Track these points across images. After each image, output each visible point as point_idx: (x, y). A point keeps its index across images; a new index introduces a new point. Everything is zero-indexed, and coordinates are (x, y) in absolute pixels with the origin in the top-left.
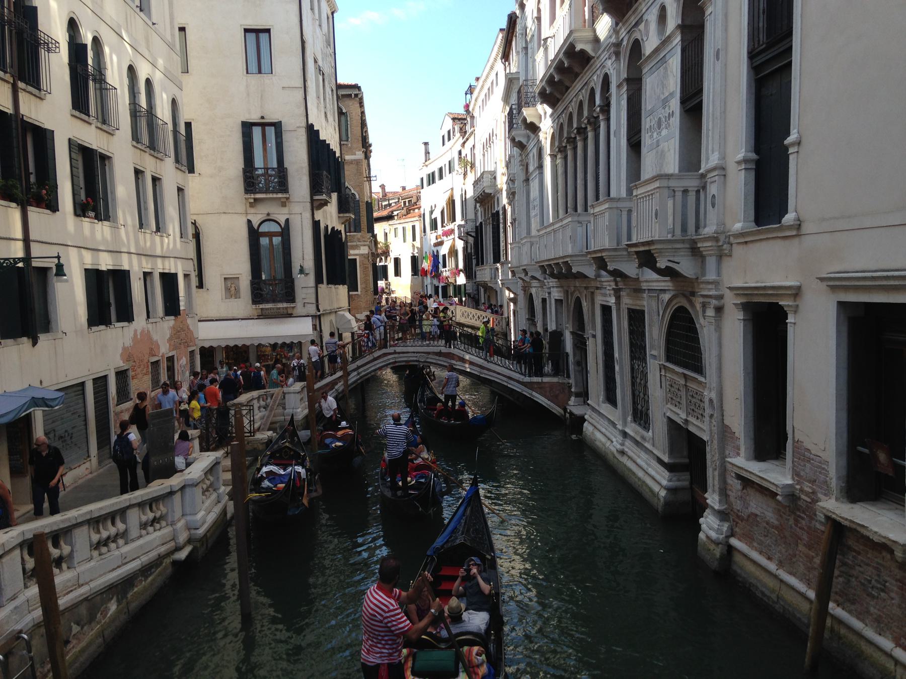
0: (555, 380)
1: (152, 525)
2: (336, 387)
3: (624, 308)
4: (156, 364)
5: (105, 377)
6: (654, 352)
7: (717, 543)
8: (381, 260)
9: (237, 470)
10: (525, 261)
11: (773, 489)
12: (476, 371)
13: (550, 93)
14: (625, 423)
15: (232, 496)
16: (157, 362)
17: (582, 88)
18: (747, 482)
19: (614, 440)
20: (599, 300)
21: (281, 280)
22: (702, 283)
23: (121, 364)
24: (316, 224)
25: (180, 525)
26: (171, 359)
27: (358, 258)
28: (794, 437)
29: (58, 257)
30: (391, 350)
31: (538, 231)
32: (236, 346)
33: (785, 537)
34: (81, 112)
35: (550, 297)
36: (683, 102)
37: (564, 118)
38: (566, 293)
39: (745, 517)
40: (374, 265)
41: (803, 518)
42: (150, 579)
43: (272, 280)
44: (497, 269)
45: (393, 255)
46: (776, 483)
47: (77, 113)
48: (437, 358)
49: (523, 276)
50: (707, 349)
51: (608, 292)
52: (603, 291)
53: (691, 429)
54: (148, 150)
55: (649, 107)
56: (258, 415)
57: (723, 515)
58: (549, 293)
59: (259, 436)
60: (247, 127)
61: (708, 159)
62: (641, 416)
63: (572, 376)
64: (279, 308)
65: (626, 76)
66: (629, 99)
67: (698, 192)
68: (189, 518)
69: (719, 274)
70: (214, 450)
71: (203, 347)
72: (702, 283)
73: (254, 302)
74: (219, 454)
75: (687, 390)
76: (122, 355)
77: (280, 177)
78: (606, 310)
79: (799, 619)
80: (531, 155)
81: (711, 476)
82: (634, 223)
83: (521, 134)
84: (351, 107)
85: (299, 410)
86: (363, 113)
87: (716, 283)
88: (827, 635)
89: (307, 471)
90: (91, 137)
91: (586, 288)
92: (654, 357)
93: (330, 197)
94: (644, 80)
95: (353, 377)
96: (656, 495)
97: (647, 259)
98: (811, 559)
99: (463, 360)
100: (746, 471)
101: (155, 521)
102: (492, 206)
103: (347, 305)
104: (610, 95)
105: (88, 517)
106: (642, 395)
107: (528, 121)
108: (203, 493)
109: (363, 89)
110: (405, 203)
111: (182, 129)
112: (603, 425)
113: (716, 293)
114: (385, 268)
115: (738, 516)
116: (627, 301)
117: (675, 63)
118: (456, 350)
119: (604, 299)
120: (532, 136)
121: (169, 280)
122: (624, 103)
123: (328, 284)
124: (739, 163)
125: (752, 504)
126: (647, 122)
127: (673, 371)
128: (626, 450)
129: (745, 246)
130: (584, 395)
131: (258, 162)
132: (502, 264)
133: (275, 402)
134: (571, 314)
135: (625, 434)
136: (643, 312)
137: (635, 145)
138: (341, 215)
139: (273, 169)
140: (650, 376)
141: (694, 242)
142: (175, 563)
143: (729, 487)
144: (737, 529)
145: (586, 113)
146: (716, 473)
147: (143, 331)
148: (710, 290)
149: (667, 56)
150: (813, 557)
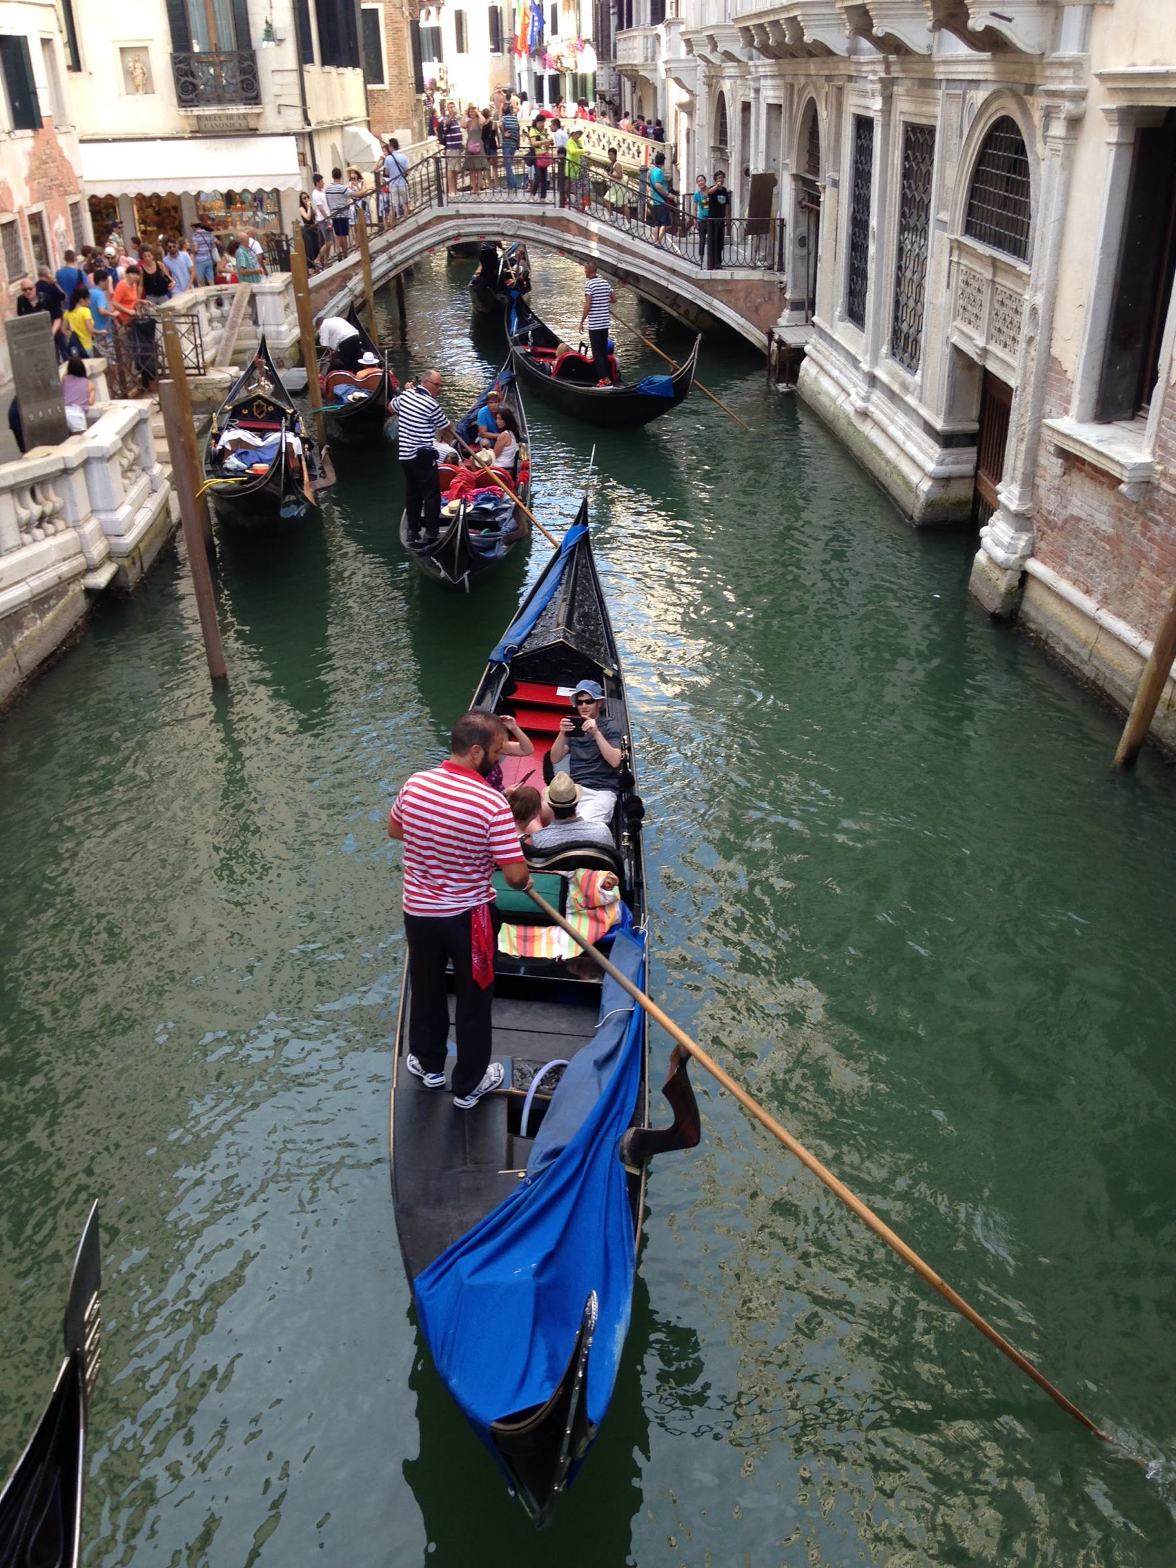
0: (757, 275)
1: (39, 526)
2: (350, 284)
3: (898, 120)
6: (944, 216)
7: (1004, 568)
9: (176, 432)
10: (713, 19)
11: (1116, 472)
12: (610, 256)
14: (875, 360)
15: (176, 481)
16: (11, 224)
18: (1072, 461)
19: (852, 391)
20: (853, 105)
21: (230, 54)
22: (1052, 64)
25: (90, 527)
26: (36, 219)
28: (1168, 378)
30: (449, 210)
32: (156, 196)
33: (1121, 556)
35: (757, 99)
39: (1060, 523)
40: (415, 24)
41: (1157, 523)
42: (49, 616)
43: (213, 55)
44: (658, 37)
46: (1122, 460)
50: (1041, 205)
51: (869, 87)
52: (860, 85)
53: (992, 367)
56: (210, 335)
57: (1022, 521)
59: (214, 375)
62: (905, 345)
63: (788, 267)
64: (231, 117)
68: (103, 516)
69: (1084, 45)
70: (138, 396)
71: (93, 197)
72: (1052, 64)
73: (183, 102)
74: (144, 404)
75: (995, 290)
79: (1120, 688)
85: (284, 328)
87: (1076, 65)
88: (1159, 712)
89: (304, 441)
91: (829, 78)
92: (943, 224)
95: (381, 265)
96: (911, 489)
98: (1156, 591)
99: (586, 233)
100: (1076, 441)
101: (43, 520)
103: (364, 112)
106: (911, 303)
112: (835, 364)
113: (1075, 87)
114: (436, 33)
115: (1047, 522)
116: (905, 108)
119: (862, 102)
123: (324, 63)
125: (1075, 500)
128: (872, 409)
130: (806, 306)
132: (668, 26)
133: (238, 308)
134: (796, 140)
135: (873, 380)
140: (930, 265)
142: (89, 592)
143: (1040, 472)
144: (1042, 545)
146: (1023, 447)
148: (1063, 79)
150: (1162, 588)
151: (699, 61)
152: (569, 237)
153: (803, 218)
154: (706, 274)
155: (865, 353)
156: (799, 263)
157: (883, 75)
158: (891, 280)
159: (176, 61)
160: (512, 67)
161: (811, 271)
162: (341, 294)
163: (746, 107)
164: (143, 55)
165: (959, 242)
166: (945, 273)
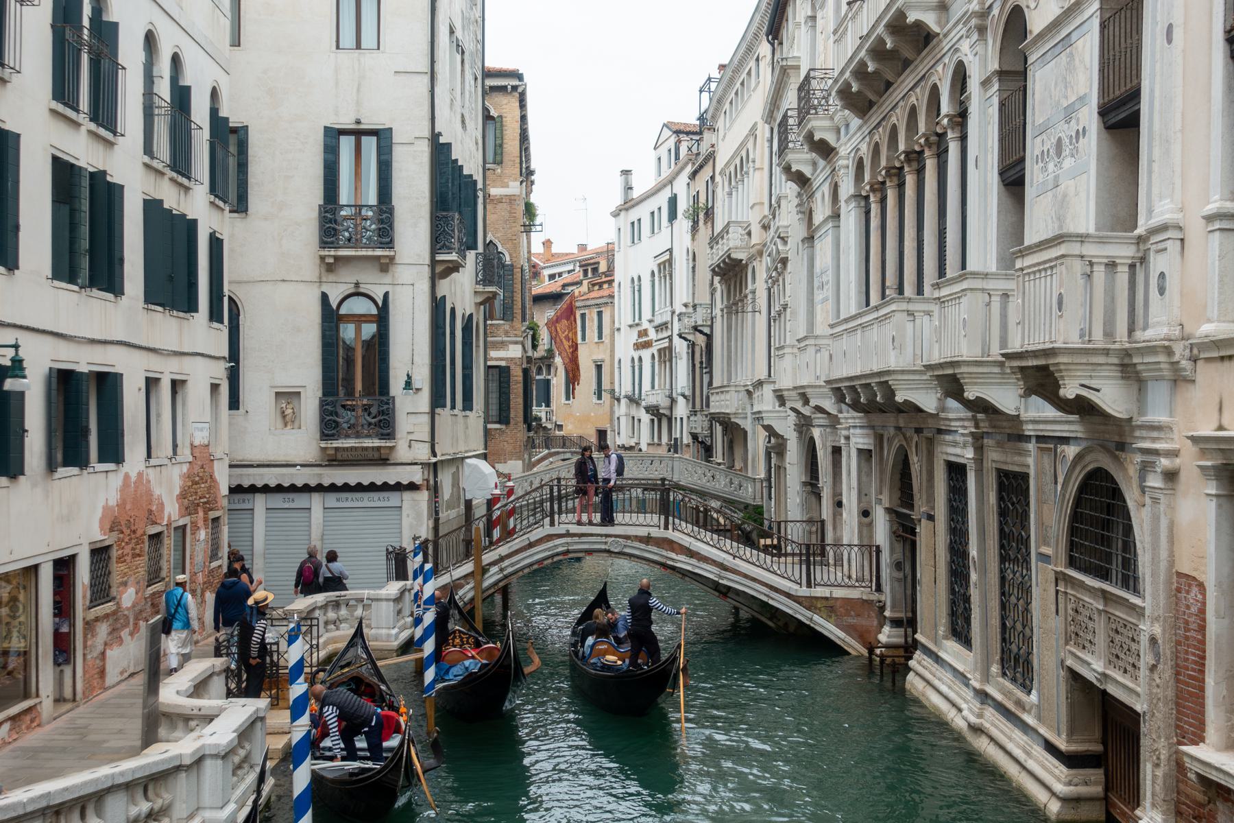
3: (988, 465)
4: (156, 538)
5: (73, 558)
8: (539, 371)
14: (986, 677)
17: (915, 85)
19: (964, 706)
23: (98, 535)
29: (16, 347)
30: (561, 529)
31: (832, 326)
34: (66, 104)
36: (1103, 112)
37: (882, 136)
38: (879, 439)
47: (60, 108)
48: (643, 546)
49: (798, 405)
52: (948, 438)
53: (1112, 689)
54: (168, 171)
55: (1040, 120)
58: (847, 438)
60: (333, 136)
61: (1150, 212)
62: (1016, 663)
63: (886, 587)
64: (366, 448)
65: (996, 67)
67: (1132, 266)
72: (1141, 427)
73: (324, 436)
76: (101, 521)
77: (381, 221)
78: (956, 471)
80: (818, 195)
81: (1149, 777)
82: (1013, 318)
83: (801, 159)
84: (506, 107)
90: (83, 151)
92: (1044, 558)
93: (464, 257)
97: (1040, 378)
104: (968, 98)
105: (44, 804)
106: (1019, 626)
107: (816, 138)
108: (234, 774)
110: (585, 272)
112: (945, 683)
116: (994, 456)
117: (1088, 46)
118: (677, 534)
120: (822, 163)
124: (1209, 219)
126: (1035, 146)
127: (1082, 585)
128: (987, 725)
129: (1219, 365)
131: (345, 195)
135: (983, 696)
136: (1025, 477)
137: (1013, 181)
139: (371, 207)
141: (1127, 353)
149: (1074, 37)
151: (790, 412)
152: (673, 555)
153: (899, 547)
154: (803, 591)
155: (975, 670)
156: (896, 584)
159: (323, 404)
160: (612, 412)
161: (909, 592)
163: (837, 451)
164: (295, 402)
165: (1064, 574)
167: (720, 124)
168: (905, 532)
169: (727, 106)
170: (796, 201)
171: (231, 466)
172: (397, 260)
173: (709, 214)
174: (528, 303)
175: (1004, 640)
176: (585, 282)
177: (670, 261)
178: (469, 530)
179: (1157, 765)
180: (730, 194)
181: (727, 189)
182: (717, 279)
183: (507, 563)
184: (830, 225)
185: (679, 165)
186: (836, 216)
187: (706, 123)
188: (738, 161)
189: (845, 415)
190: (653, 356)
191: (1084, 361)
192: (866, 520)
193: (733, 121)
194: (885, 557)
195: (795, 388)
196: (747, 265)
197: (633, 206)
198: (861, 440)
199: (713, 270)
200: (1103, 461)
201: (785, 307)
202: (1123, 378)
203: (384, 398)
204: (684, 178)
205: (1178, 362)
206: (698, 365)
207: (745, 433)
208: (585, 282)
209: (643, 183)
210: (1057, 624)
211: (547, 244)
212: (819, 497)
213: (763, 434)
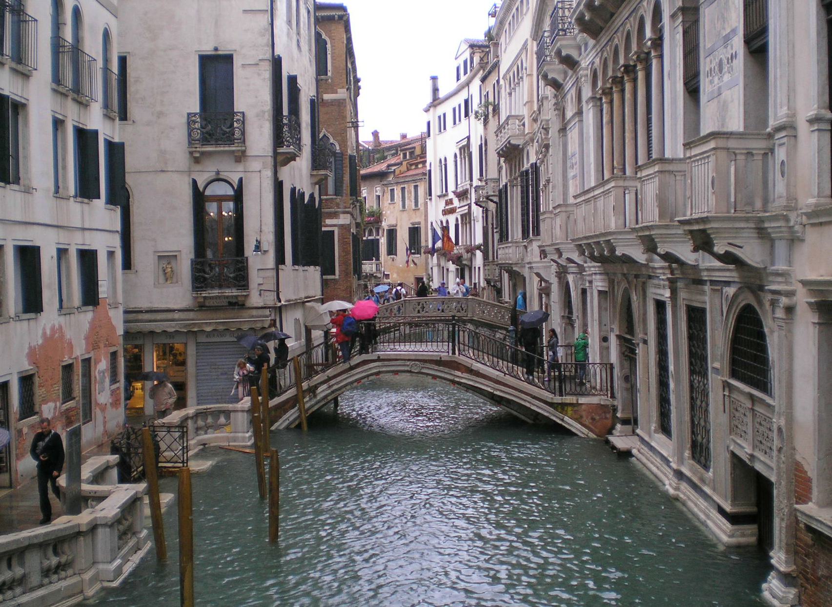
6: (717, 365)
13: (591, 20)
14: (681, 461)
23: (26, 366)
24: (278, 186)
26: (87, 362)
27: (336, 230)
31: (575, 197)
37: (608, 53)
38: (611, 282)
45: (385, 225)
48: (436, 367)
49: (555, 257)
52: (655, 281)
53: (758, 467)
55: (708, 45)
62: (700, 451)
63: (618, 395)
66: (685, 33)
69: (790, 263)
80: (569, 97)
83: (556, 70)
86: (349, 40)
91: (637, 276)
94: (701, 11)
102: (520, 163)
104: (662, 27)
106: (702, 423)
107: (563, 54)
108: (120, 538)
109: (349, 11)
110: (405, 155)
111: (115, 67)
118: (462, 357)
120: (570, 72)
121: (88, 258)
122: (679, 37)
123: (295, 262)
126: (705, 65)
129: (817, 229)
130: (631, 422)
135: (679, 475)
137: (692, 90)
138: (315, 173)
141: (761, 220)
145: (634, 47)
146: (784, 525)
147: (53, 328)
152: (459, 373)
153: (627, 364)
154: (558, 399)
156: (625, 393)
157: (669, 276)
158: (687, 406)
159: (194, 263)
160: (427, 264)
162: (293, 411)
163: (584, 292)
166: (721, 403)
167: (502, 40)
168: (629, 352)
169: (507, 26)
170: (553, 101)
171: (126, 312)
172: (250, 153)
173: (496, 110)
174: (359, 180)
175: (693, 433)
176: (405, 163)
177: (468, 145)
178: (310, 357)
179: (783, 519)
180: (510, 94)
181: (508, 90)
182: (502, 159)
183: (332, 382)
184: (577, 119)
185: (474, 71)
186: (580, 113)
187: (492, 37)
188: (515, 68)
189: (590, 264)
190: (457, 219)
191: (731, 226)
192: (605, 344)
193: (511, 38)
194: (616, 371)
195: (552, 245)
196: (523, 149)
197: (440, 104)
198: (600, 284)
199: (498, 153)
200: (748, 299)
201: (548, 181)
202: (759, 238)
203: (239, 259)
204: (477, 82)
205: (793, 227)
206: (490, 226)
207: (524, 278)
208: (405, 163)
209: (447, 86)
210: (724, 419)
211: (376, 134)
212: (573, 327)
213: (536, 279)
